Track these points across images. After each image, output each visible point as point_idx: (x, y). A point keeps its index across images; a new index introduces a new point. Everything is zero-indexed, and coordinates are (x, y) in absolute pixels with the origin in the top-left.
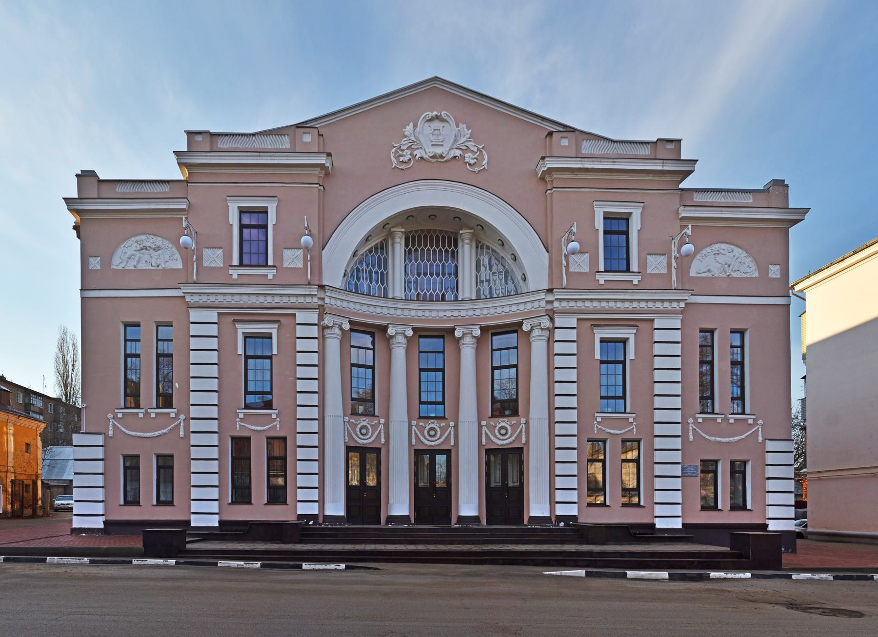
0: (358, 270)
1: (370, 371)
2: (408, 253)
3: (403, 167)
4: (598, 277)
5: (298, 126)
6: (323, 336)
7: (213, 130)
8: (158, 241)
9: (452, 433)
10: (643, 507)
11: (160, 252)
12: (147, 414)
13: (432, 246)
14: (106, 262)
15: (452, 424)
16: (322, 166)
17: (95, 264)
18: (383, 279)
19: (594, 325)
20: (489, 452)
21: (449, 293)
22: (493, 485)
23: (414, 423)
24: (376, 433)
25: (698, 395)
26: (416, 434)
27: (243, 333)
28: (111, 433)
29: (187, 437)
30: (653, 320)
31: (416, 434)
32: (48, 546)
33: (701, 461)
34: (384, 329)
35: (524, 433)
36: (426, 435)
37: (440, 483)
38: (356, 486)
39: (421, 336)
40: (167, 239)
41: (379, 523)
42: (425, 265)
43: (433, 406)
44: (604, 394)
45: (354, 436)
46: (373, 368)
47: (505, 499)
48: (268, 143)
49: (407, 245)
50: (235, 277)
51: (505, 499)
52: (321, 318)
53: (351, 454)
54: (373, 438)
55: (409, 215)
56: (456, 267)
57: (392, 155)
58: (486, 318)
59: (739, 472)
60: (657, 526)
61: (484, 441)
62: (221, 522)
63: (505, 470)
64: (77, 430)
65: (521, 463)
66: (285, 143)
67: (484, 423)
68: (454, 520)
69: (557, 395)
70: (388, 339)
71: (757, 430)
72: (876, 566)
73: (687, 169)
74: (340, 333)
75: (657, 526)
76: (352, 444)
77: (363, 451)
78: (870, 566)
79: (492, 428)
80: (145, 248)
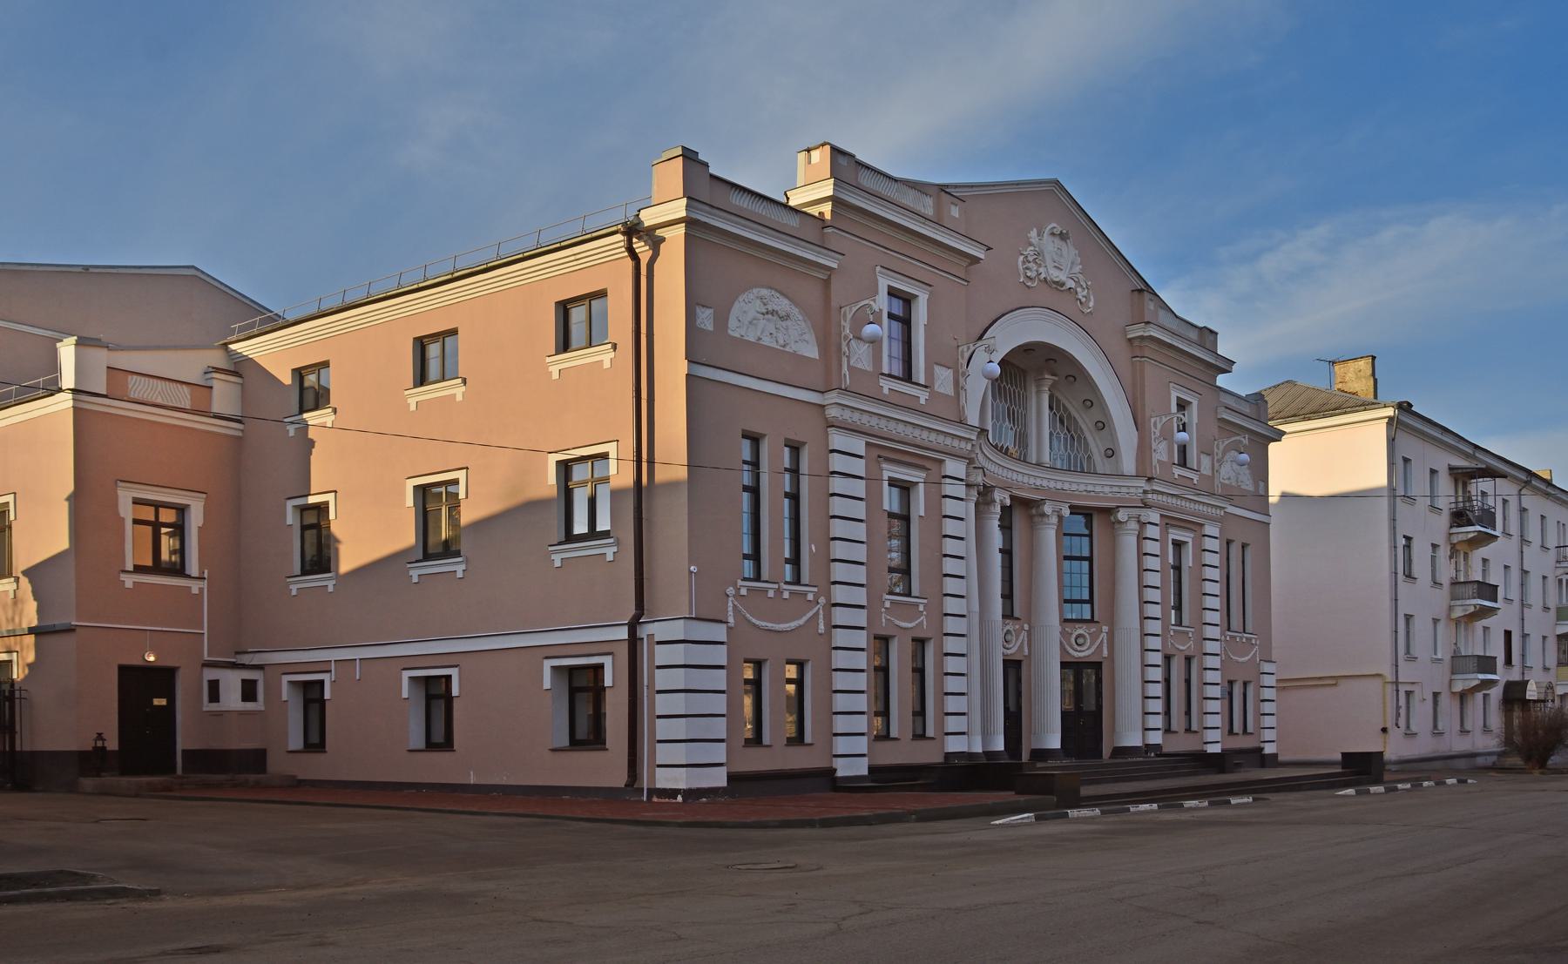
1: (1086, 564)
2: (226, 436)
4: (123, 577)
5: (943, 188)
7: (859, 157)
8: (783, 305)
10: (789, 662)
11: (789, 323)
12: (779, 592)
14: (721, 320)
16: (1006, 511)
17: (705, 318)
19: (1408, 652)
22: (132, 379)
27: (327, 503)
28: (731, 620)
29: (828, 635)
30: (941, 461)
32: (1002, 793)
33: (914, 640)
34: (1108, 511)
38: (113, 752)
40: (797, 305)
41: (1101, 756)
43: (1092, 602)
44: (1068, 597)
47: (1084, 723)
48: (909, 198)
50: (886, 391)
51: (1084, 723)
58: (1078, 497)
59: (438, 697)
60: (840, 774)
62: (872, 769)
63: (1087, 683)
64: (1391, 419)
66: (927, 206)
68: (1106, 751)
69: (659, 692)
71: (817, 613)
72: (8, 910)
73: (1226, 366)
75: (840, 774)
78: (712, 819)
80: (773, 313)
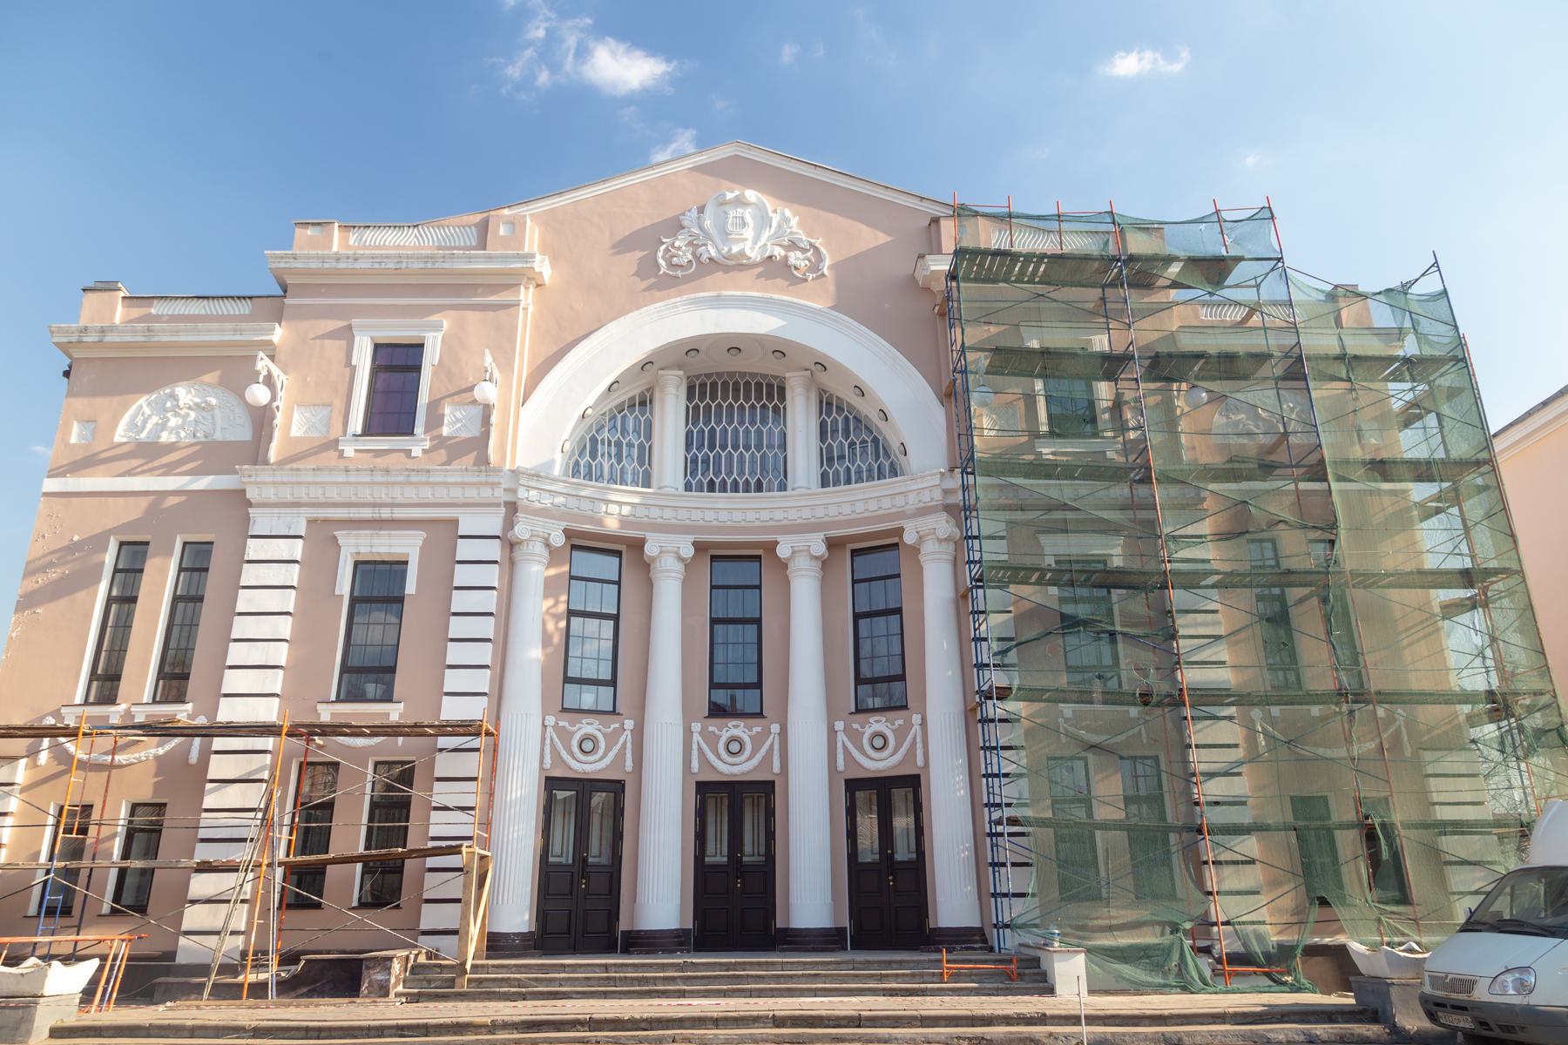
0: (594, 440)
2: (693, 415)
3: (679, 273)
6: (511, 559)
9: (776, 747)
13: (736, 399)
15: (629, 724)
18: (645, 455)
20: (853, 786)
21: (770, 475)
23: (696, 727)
24: (615, 750)
25: (206, 607)
26: (700, 749)
31: (700, 749)
35: (919, 745)
36: (576, 749)
37: (903, 853)
39: (574, 547)
42: (736, 431)
45: (565, 755)
46: (616, 618)
49: (690, 397)
52: (509, 524)
53: (860, 795)
54: (608, 760)
55: (692, 348)
56: (784, 435)
57: (660, 254)
61: (548, 764)
65: (770, 813)
67: (839, 725)
70: (645, 567)
74: (546, 553)
76: (558, 773)
77: (584, 787)
79: (855, 737)
